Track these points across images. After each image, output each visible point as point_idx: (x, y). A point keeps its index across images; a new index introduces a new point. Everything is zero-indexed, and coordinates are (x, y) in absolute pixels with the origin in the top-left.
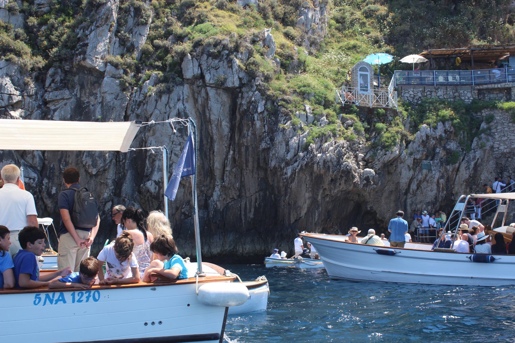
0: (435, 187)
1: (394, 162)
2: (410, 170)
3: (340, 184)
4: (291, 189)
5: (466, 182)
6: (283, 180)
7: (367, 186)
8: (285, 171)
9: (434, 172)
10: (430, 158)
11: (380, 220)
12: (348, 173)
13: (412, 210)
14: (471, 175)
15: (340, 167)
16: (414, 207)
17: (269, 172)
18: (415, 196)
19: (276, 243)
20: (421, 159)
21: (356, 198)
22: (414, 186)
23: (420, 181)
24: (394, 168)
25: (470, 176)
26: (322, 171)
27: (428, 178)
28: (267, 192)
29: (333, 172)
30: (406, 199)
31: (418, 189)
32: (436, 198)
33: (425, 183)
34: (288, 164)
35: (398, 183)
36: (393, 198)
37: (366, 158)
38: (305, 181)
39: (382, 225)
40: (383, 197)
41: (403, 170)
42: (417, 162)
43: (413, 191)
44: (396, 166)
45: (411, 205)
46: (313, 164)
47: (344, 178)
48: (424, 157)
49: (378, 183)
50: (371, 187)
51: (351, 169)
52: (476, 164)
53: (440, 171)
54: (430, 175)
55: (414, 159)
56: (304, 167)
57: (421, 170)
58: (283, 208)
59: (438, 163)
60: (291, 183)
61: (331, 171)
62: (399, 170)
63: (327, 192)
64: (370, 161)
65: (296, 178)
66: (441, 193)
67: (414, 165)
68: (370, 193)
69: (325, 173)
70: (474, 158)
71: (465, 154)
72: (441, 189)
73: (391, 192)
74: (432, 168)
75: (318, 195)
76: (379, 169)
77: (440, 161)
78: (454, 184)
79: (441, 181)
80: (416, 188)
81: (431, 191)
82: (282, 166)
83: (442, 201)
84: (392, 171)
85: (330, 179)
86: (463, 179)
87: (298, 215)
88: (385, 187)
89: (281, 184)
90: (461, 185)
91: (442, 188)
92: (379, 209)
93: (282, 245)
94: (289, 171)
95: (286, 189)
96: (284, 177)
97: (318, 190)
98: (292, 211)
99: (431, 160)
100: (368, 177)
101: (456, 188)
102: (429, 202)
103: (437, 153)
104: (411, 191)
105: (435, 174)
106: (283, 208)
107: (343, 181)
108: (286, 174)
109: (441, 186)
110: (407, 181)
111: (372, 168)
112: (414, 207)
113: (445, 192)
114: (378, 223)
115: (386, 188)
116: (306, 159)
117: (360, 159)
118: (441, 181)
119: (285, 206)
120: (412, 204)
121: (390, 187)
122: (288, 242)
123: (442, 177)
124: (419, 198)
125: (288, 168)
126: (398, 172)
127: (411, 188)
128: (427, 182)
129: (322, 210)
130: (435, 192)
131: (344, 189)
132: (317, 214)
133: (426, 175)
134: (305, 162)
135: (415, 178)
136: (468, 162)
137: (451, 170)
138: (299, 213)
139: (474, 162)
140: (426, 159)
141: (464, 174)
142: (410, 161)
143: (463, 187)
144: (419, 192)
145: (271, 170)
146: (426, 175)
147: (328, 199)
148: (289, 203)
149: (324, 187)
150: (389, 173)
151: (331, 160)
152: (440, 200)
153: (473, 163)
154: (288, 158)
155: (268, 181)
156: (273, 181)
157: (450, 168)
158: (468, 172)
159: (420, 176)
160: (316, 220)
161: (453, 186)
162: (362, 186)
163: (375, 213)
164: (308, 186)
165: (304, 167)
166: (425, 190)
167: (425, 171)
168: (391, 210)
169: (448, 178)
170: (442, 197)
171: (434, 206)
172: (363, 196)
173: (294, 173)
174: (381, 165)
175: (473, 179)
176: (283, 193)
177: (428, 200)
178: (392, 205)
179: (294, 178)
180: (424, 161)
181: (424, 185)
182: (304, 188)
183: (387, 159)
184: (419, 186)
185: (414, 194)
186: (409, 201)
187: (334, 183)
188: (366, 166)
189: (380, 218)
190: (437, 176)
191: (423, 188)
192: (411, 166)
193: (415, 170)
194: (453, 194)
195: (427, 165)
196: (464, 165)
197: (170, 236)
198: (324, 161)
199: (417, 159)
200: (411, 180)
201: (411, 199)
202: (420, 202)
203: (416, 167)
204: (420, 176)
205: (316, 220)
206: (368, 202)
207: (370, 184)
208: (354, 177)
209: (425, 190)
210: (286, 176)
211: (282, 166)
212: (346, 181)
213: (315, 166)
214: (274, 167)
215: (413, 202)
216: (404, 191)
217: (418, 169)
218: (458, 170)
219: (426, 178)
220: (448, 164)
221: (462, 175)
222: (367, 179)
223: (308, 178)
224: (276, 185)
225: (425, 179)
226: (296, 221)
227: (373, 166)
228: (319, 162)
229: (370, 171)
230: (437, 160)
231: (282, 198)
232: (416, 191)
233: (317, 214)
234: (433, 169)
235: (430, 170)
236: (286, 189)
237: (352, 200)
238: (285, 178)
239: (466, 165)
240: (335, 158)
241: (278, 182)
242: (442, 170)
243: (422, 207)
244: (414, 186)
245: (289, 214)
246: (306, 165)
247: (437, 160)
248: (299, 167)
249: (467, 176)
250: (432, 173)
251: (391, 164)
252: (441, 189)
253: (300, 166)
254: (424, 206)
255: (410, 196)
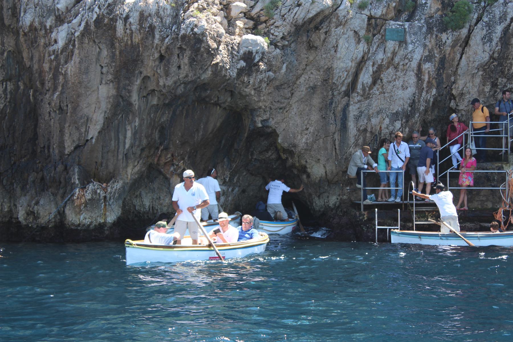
0: (412, 79)
1: (322, 22)
2: (359, 42)
3: (179, 67)
4: (65, 75)
5: (484, 70)
6: (50, 55)
7: (249, 75)
8: (53, 35)
9: (410, 47)
10: (404, 16)
11: (285, 151)
12: (196, 44)
13: (359, 130)
14: (496, 55)
15: (179, 28)
16: (363, 122)
17: (22, 39)
18: (367, 98)
19: (28, 197)
20: (384, 19)
21: (226, 99)
22: (366, 78)
23: (380, 67)
24: (323, 37)
25: (491, 57)
26: (137, 38)
27: (396, 60)
28: (21, 84)
29: (163, 39)
30: (348, 105)
31: (374, 83)
32: (413, 104)
33: (391, 70)
34: (60, 20)
35: (329, 70)
36: (316, 101)
37: (254, 12)
38: (98, 60)
39: (291, 160)
40: (294, 99)
41: (341, 42)
42: (377, 25)
43: (364, 89)
44: (326, 33)
45: (357, 118)
46: (114, 20)
47: (188, 53)
48: (392, 14)
49: (280, 68)
50: (260, 77)
51: (203, 34)
52: (506, 30)
53: (425, 46)
54: (401, 53)
55: (370, 18)
56: (92, 27)
57: (383, 41)
58: (47, 118)
59: (420, 28)
60: (66, 62)
61: (157, 36)
62: (332, 40)
63: (151, 86)
64: (263, 18)
65: (76, 51)
66: (424, 94)
67: (368, 30)
68: (258, 90)
69: (144, 39)
70: (503, 17)
71: (485, 7)
72: (425, 85)
73: (314, 88)
74: (408, 37)
75: (130, 92)
76: (283, 38)
77: (427, 22)
78: (455, 73)
79: (427, 66)
80: (370, 81)
81: (404, 88)
82: (48, 25)
83: (426, 111)
84: (318, 43)
85: (157, 55)
86: (477, 64)
87: (81, 134)
88: (298, 78)
89: (46, 66)
90: (473, 76)
91: (429, 82)
92: (283, 125)
93: (42, 202)
94: (61, 35)
95: (55, 77)
96: (51, 49)
97: (129, 79)
98: (67, 125)
99: (407, 21)
100: (250, 53)
101: (461, 83)
102: (397, 113)
103: (421, 5)
104: (359, 86)
105: (413, 51)
106: (47, 118)
107: (186, 60)
108: (56, 41)
109: (426, 78)
110: (351, 65)
111: (265, 34)
112: (363, 122)
113: (434, 91)
114: (284, 156)
115: (302, 80)
116: (97, 9)
117: (234, 13)
118: (427, 66)
119: (53, 114)
120: (360, 116)
121: (314, 77)
122: (54, 195)
123: (429, 58)
124: (376, 103)
125: (60, 28)
126: (330, 46)
127: (360, 80)
128: (396, 68)
129: (140, 125)
130: (412, 90)
131: (190, 79)
132: (129, 134)
133: (394, 54)
134: (95, 16)
135: (369, 59)
136: (489, 26)
137: (449, 42)
138: (83, 130)
139: (503, 25)
140: (396, 18)
141: (480, 52)
142: (359, 22)
143: (478, 80)
144: (375, 90)
145: (25, 34)
146: (394, 54)
147: (155, 102)
148: (60, 108)
149: (145, 73)
150: (311, 47)
151: (157, 13)
152: (422, 108)
153: (499, 29)
154: (59, 6)
155: (23, 58)
156: (32, 59)
157: (447, 38)
158: (487, 47)
159: (380, 56)
160: (127, 146)
161: (453, 79)
162: (234, 73)
163: (274, 134)
164: (105, 70)
165: (92, 27)
166: (390, 87)
167: (391, 45)
168: (311, 129)
169: (443, 60)
170: (427, 101)
171: (407, 121)
172: (243, 97)
173: (70, 41)
174: (288, 28)
175: (500, 64)
176: (48, 85)
177: (396, 108)
178: (315, 117)
179: (72, 52)
180: (392, 22)
181: (387, 75)
182: (94, 75)
183: (302, 16)
184: (376, 78)
185: (366, 95)
186: (353, 111)
187: (165, 65)
188: (254, 30)
189: (286, 145)
190: (417, 57)
191: (385, 80)
192: (362, 33)
193: (369, 42)
194: (453, 97)
195: (397, 31)
196: (479, 33)
197: (288, 189)
198: (142, 14)
199: (376, 19)
200: (361, 64)
201: (357, 106)
202: (378, 113)
203: (374, 35)
204: (380, 56)
205: (127, 146)
206: (254, 110)
207: (258, 70)
208: (212, 53)
209: (390, 87)
210: (55, 47)
211: (48, 25)
212: (192, 61)
213: (120, 25)
214: (31, 26)
215: (361, 112)
216: (344, 88)
217: (376, 39)
218: (466, 42)
219: (392, 59)
220: (444, 30)
221: (476, 53)
222: (248, 57)
223: (105, 53)
224: (36, 67)
225: (391, 62)
226: (77, 147)
227: (269, 31)
228: (127, 17)
229: (255, 41)
230: (419, 20)
231: (48, 96)
232: (371, 88)
233: (129, 134)
234: (409, 40)
235: (403, 42)
236: (55, 77)
237: (216, 104)
238: (54, 51)
239: (484, 32)
240: (169, 7)
241: (41, 61)
242: (430, 43)
243: (381, 123)
244: (366, 78)
245: (62, 132)
246: (98, 21)
247: (419, 20)
248: (82, 28)
249: (486, 57)
250: (406, 48)
251: (317, 28)
252: (425, 85)
253: (83, 24)
254: (387, 121)
255: (356, 99)
